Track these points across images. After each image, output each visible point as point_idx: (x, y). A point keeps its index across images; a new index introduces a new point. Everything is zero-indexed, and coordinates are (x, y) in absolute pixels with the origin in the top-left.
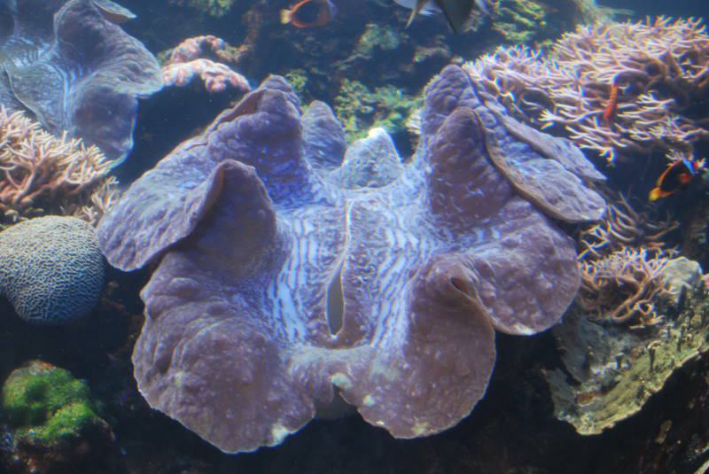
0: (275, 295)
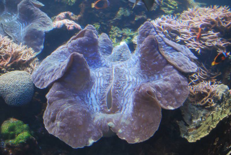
0: (90, 96)
